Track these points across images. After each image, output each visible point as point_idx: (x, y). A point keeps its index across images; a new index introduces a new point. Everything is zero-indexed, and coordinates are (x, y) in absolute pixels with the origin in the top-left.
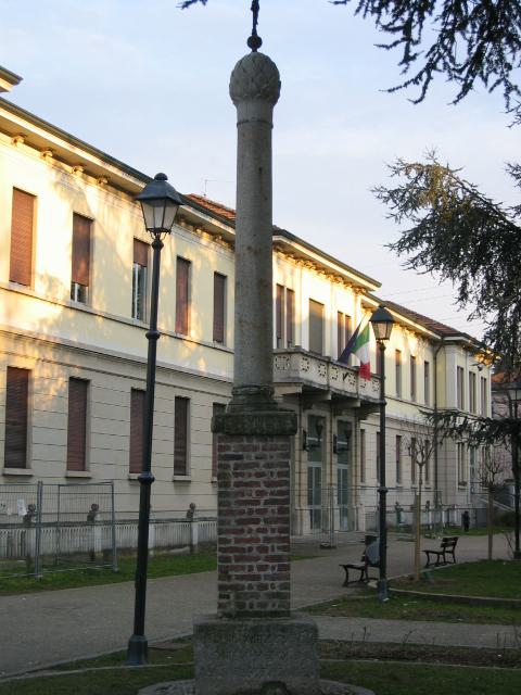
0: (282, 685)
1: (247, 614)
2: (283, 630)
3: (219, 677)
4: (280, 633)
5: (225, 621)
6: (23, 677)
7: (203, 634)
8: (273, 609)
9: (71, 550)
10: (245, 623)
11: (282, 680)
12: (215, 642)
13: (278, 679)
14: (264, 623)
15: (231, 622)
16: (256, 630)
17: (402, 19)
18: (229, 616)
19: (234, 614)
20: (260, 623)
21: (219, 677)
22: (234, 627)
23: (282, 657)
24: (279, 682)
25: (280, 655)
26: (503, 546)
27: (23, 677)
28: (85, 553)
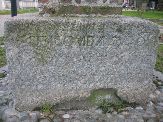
0: (114, 92)
1: (74, 10)
2: (119, 31)
3: (40, 87)
4: (116, 33)
5: (46, 17)
6: (148, 16)
7: (14, 35)
8: (104, 5)
9: (30, 7)
10: (71, 20)
11: (114, 87)
12: (32, 45)
13: (110, 85)
14: (97, 20)
15: (54, 19)
16: (85, 29)
17: (108, 20)
18: (52, 11)
19: (57, 10)
20: (92, 21)
21: (40, 87)
22: (57, 25)
23: (116, 63)
24: (111, 89)
25: (115, 59)
26: (1, 81)
27: (148, 16)
28: (33, 7)
